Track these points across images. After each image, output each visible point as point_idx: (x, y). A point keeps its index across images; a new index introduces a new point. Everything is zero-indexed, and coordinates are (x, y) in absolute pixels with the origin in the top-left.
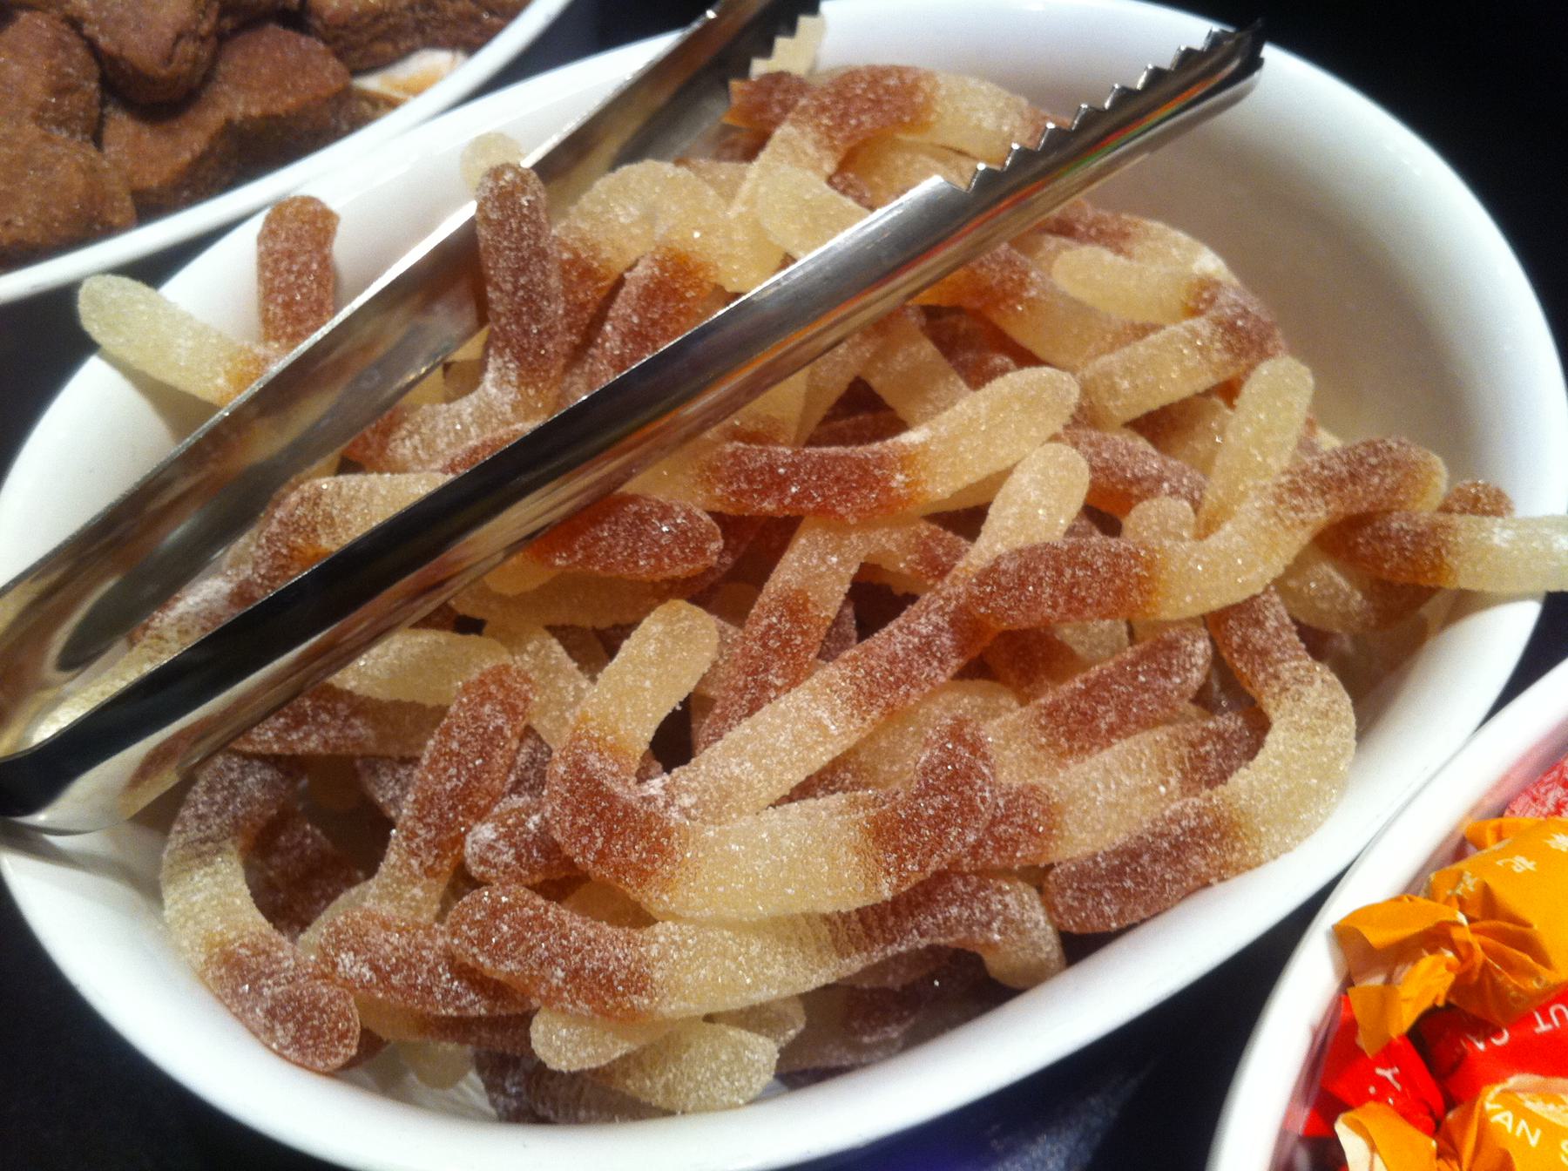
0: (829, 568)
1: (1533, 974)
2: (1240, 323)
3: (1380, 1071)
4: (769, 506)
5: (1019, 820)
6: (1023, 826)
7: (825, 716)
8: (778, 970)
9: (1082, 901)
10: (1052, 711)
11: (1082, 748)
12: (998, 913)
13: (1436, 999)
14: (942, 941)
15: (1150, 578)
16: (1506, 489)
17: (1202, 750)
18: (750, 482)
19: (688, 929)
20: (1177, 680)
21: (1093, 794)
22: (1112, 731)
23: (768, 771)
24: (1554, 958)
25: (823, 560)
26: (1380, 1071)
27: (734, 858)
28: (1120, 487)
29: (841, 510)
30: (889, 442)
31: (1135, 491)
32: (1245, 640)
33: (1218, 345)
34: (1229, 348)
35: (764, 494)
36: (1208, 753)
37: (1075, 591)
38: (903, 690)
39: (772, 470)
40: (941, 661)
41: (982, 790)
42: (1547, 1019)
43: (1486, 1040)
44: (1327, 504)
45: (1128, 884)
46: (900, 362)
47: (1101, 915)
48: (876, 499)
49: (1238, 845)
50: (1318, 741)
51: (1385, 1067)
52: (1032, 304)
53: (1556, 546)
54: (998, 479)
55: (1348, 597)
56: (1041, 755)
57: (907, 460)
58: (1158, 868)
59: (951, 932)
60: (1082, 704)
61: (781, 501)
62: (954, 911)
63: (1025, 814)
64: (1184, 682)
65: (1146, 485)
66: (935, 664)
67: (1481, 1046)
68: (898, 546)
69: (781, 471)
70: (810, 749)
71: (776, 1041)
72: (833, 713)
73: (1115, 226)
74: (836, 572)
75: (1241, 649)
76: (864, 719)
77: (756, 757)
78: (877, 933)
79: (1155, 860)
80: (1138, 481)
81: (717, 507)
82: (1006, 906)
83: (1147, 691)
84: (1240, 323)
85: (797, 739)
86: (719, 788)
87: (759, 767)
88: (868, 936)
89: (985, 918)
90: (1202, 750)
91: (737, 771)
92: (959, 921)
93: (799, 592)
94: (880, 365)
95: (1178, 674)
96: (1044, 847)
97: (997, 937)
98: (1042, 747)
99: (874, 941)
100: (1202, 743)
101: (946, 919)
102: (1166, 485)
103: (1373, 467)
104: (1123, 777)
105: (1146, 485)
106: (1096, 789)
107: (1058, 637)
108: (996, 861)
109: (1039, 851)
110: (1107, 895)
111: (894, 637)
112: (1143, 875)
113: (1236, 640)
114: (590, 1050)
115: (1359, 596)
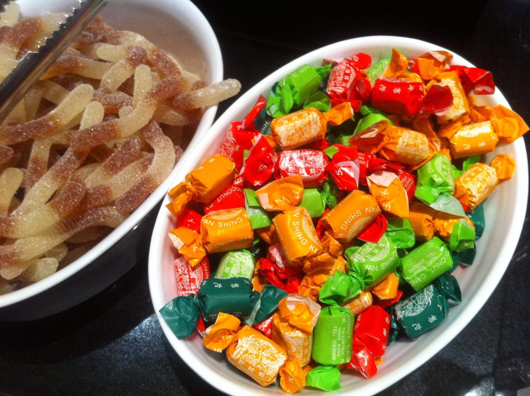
0: (42, 149)
1: (203, 190)
2: (134, 58)
3: (189, 221)
4: (20, 140)
5: (98, 193)
6: (99, 194)
7: (46, 184)
8: (45, 242)
9: (122, 206)
10: (105, 166)
11: (115, 172)
12: (101, 215)
13: (184, 201)
14: (88, 225)
15: (113, 129)
16: (322, 59)
17: (145, 164)
18: (13, 135)
19: (22, 240)
20: (133, 150)
21: (117, 182)
22: (121, 166)
23: (36, 201)
24: (207, 186)
25: (39, 148)
26: (189, 221)
27: (25, 222)
28: (114, 107)
29: (39, 135)
30: (48, 115)
31: (118, 107)
32: (148, 136)
33: (128, 65)
34: (131, 65)
35: (17, 137)
36: (146, 164)
37: (96, 137)
38: (65, 172)
39: (18, 131)
40: (74, 163)
41: (79, 189)
42: (220, 199)
43: (209, 207)
44: (155, 99)
45: (130, 199)
46: (51, 92)
47: (128, 208)
48: (47, 130)
49: (151, 183)
50: (163, 154)
51: (190, 219)
52: (83, 67)
53: (211, 92)
54: (80, 116)
55: (178, 117)
56: (106, 177)
57: (52, 118)
58: (135, 193)
59: (89, 222)
60: (112, 162)
61: (22, 138)
62: (89, 217)
63: (99, 191)
64: (135, 149)
65: (119, 105)
66: (72, 164)
67: (208, 209)
68: (60, 138)
69: (20, 131)
70: (45, 193)
71: (57, 259)
72: (48, 183)
73: (116, 35)
74: (44, 150)
75: (147, 138)
76: (57, 182)
77: (33, 198)
78: (70, 228)
79: (134, 192)
80: (117, 104)
81: (8, 144)
82: (104, 213)
83: (126, 154)
84: (134, 58)
85: (41, 191)
86: (27, 208)
87: (33, 200)
88: (68, 229)
89: (98, 217)
90: (145, 164)
91: (29, 203)
92: (90, 219)
93: (36, 157)
94: (47, 95)
95: (132, 148)
96: (108, 197)
97: (103, 220)
98: (106, 175)
99: (69, 229)
100: (144, 162)
101: (87, 220)
102: (124, 104)
103: (165, 86)
104: (125, 176)
105: (119, 105)
106: (118, 181)
107: (108, 148)
108: (96, 204)
109: (107, 198)
110: (127, 203)
111: (62, 161)
112: (133, 196)
113: (146, 136)
114: (13, 272)
115: (181, 116)
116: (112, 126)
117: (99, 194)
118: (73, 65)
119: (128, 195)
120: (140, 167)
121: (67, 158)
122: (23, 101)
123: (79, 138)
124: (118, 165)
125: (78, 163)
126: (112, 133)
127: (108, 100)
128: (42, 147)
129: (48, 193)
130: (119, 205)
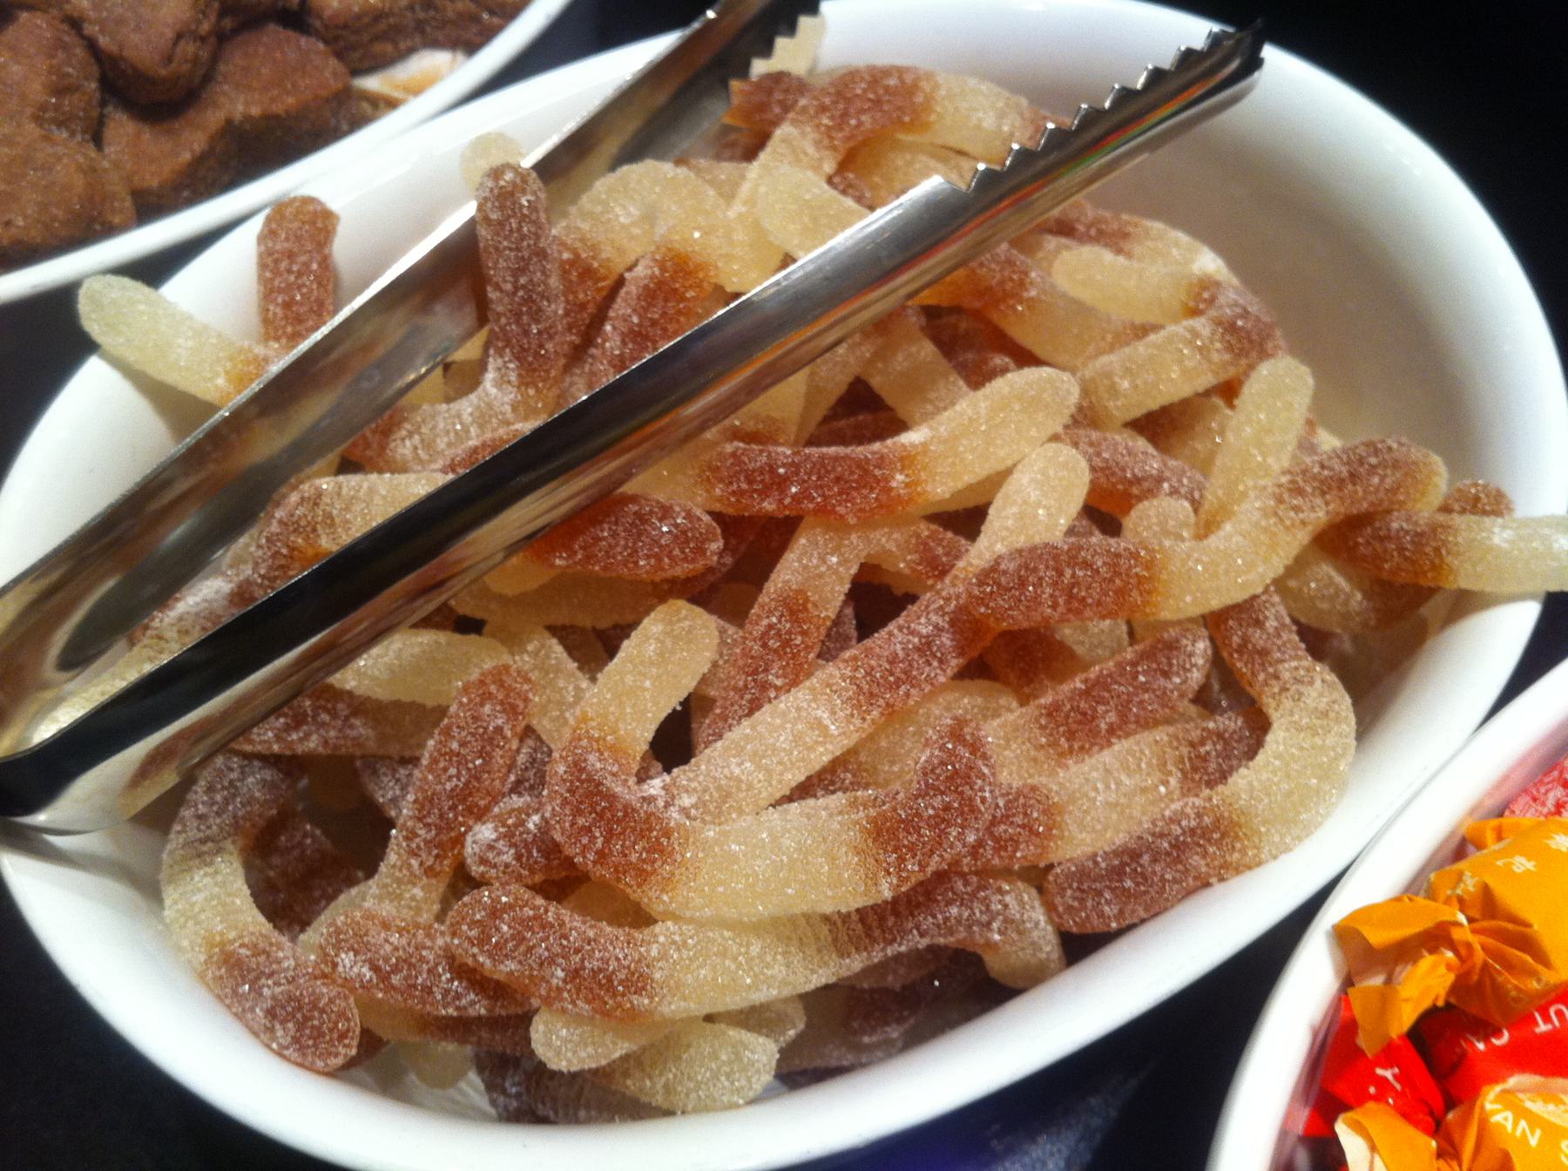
1: (1533, 974)
2: (1240, 323)
3: (1380, 1071)
4: (769, 506)
5: (1019, 820)
7: (825, 716)
8: (778, 970)
9: (1082, 901)
10: (1052, 711)
11: (1082, 748)
12: (998, 913)
13: (1436, 999)
14: (942, 941)
15: (1150, 578)
17: (1202, 750)
18: (750, 482)
19: (688, 929)
20: (1177, 680)
21: (1093, 794)
22: (1112, 731)
23: (768, 771)
24: (1554, 958)
25: (823, 560)
26: (1380, 1071)
27: (734, 858)
28: (1120, 487)
29: (841, 510)
30: (889, 442)
31: (1135, 491)
32: (1245, 640)
33: (1218, 345)
34: (1229, 348)
35: (764, 494)
36: (1208, 753)
37: (1075, 591)
38: (903, 690)
39: (772, 470)
40: (941, 661)
41: (982, 790)
42: (1547, 1019)
43: (1486, 1040)
44: (1327, 504)
45: (1128, 884)
46: (900, 362)
47: (1101, 915)
48: (876, 499)
50: (1318, 741)
51: (1385, 1067)
52: (1032, 304)
53: (1556, 546)
54: (998, 479)
55: (1348, 597)
56: (1041, 755)
57: (907, 460)
58: (1158, 868)
59: (951, 932)
60: (1082, 704)
61: (781, 501)
62: (954, 911)
63: (1025, 814)
64: (1184, 682)
65: (1146, 485)
66: (935, 664)
67: (1481, 1046)
69: (781, 471)
70: (810, 749)
71: (776, 1041)
72: (833, 713)
73: (1115, 226)
74: (836, 572)
75: (1241, 649)
76: (864, 719)
77: (756, 757)
78: (877, 933)
79: (1155, 860)
80: (1138, 481)
81: (717, 507)
84: (1240, 323)
85: (797, 739)
87: (759, 767)
88: (868, 936)
89: (985, 918)
90: (1202, 750)
91: (737, 771)
92: (959, 921)
93: (799, 592)
94: (880, 365)
95: (1178, 674)
96: (1044, 847)
97: (997, 937)
98: (1042, 747)
99: (874, 941)
101: (946, 919)
102: (1166, 485)
103: (1373, 467)
104: (1123, 777)
105: (1146, 485)
106: (1096, 789)
107: (1058, 637)
108: (996, 861)
109: (1039, 851)
110: (1107, 895)
111: (894, 637)
112: (1143, 875)
114: (590, 1050)
115: (1359, 596)
117: (1023, 826)
118: (1009, 286)
119: (1124, 864)
120: (1182, 757)
121: (921, 636)
123: (1020, 577)
124: (1103, 726)
125: (955, 663)
126: (1135, 593)
128: (835, 559)
129: (822, 754)
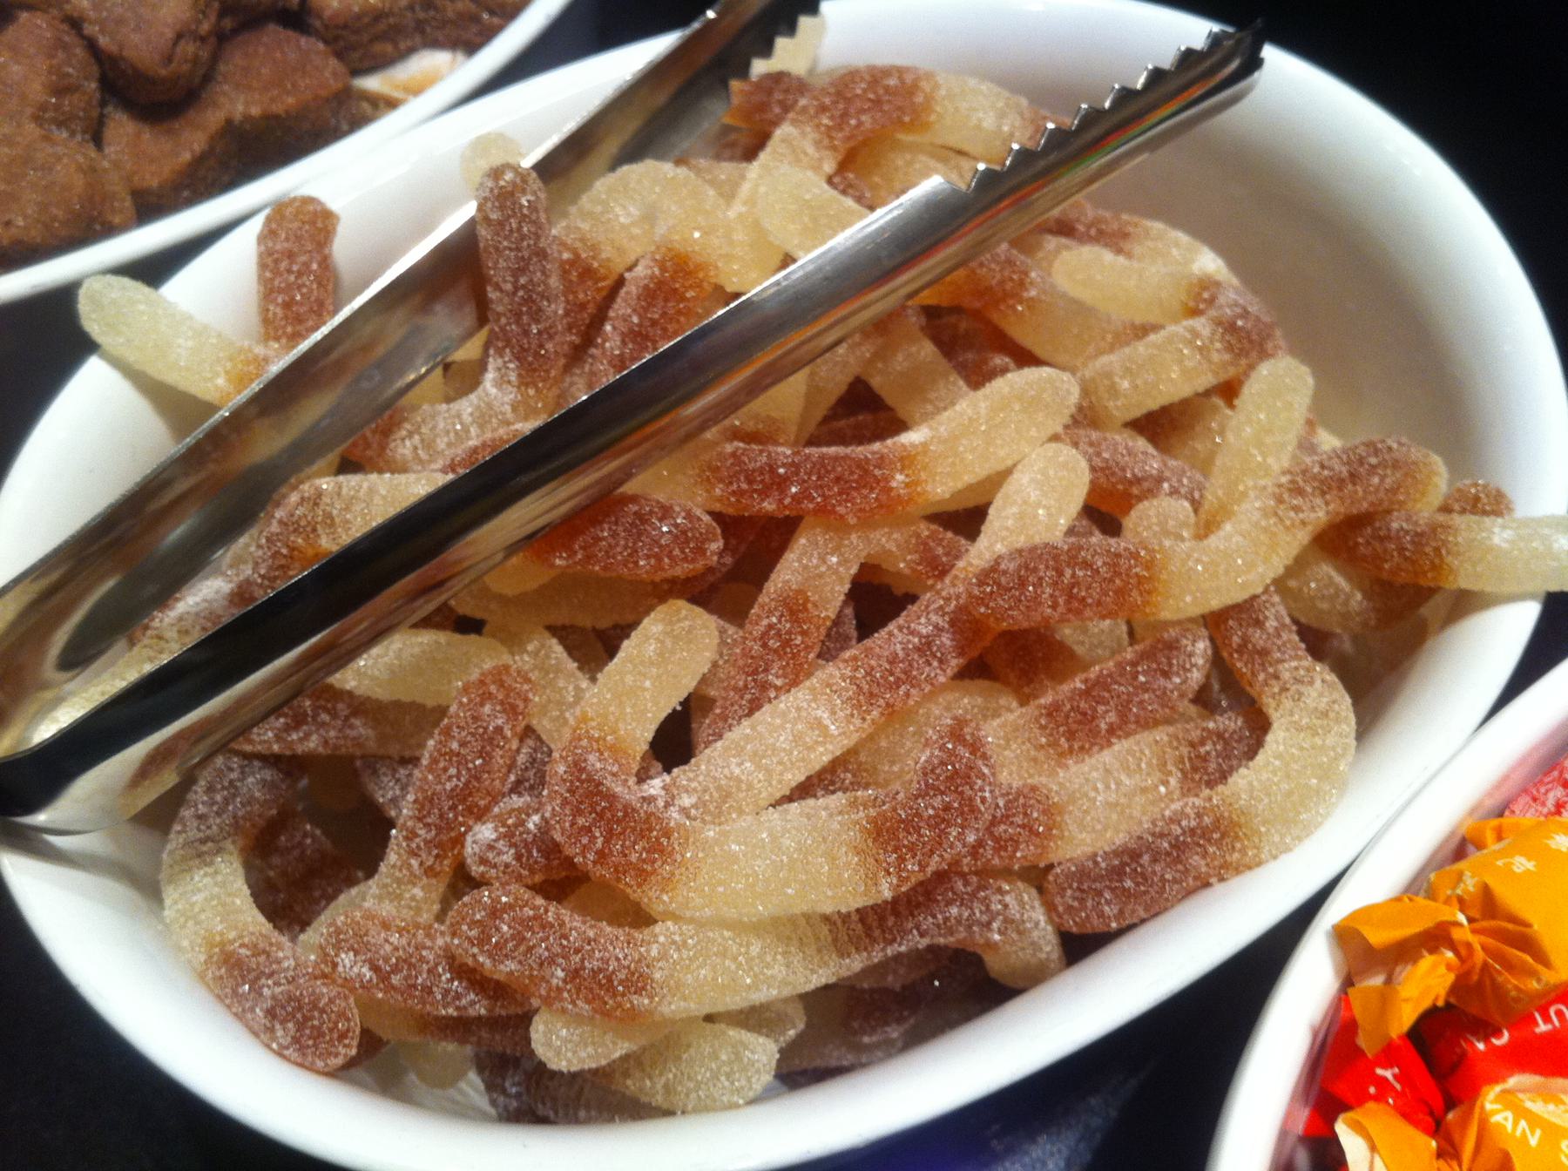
0: (829, 568)
1: (1533, 974)
2: (1240, 323)
3: (1380, 1071)
4: (769, 506)
5: (1019, 820)
6: (1023, 826)
7: (825, 716)
8: (778, 970)
9: (1082, 901)
10: (1052, 711)
11: (1082, 748)
12: (998, 913)
13: (1436, 999)
14: (942, 941)
15: (1150, 578)
17: (1202, 750)
19: (688, 929)
20: (1177, 680)
22: (1112, 731)
23: (768, 771)
24: (1554, 958)
25: (823, 560)
26: (1380, 1071)
27: (734, 858)
28: (1120, 487)
29: (841, 510)
30: (889, 442)
31: (1135, 491)
32: (1245, 640)
33: (1218, 345)
34: (1229, 348)
35: (764, 494)
37: (1075, 591)
38: (903, 690)
39: (772, 470)
40: (941, 661)
41: (982, 790)
42: (1547, 1019)
43: (1486, 1040)
44: (1327, 504)
45: (1128, 884)
46: (900, 362)
47: (1101, 915)
48: (876, 499)
49: (1238, 845)
50: (1318, 741)
51: (1385, 1067)
52: (1032, 304)
53: (1556, 546)
54: (998, 479)
55: (1348, 597)
56: (1041, 755)
57: (907, 460)
58: (1158, 868)
59: (951, 932)
60: (1082, 704)
61: (781, 501)
62: (954, 911)
63: (1025, 814)
64: (1184, 682)
65: (1146, 485)
66: (935, 664)
67: (1481, 1046)
70: (810, 749)
71: (776, 1041)
72: (833, 713)
73: (1115, 226)
74: (836, 572)
75: (1241, 649)
76: (864, 719)
77: (756, 757)
78: (877, 933)
79: (1155, 860)
80: (1138, 481)
81: (717, 507)
82: (1006, 906)
83: (1147, 691)
84: (1240, 323)
85: (797, 739)
86: (719, 788)
87: (759, 767)
88: (868, 936)
89: (985, 918)
90: (1202, 750)
91: (737, 771)
92: (959, 921)
94: (880, 365)
95: (1178, 674)
96: (1044, 847)
97: (997, 937)
98: (1042, 747)
99: (874, 941)
100: (1202, 743)
101: (946, 919)
102: (1166, 485)
103: (1373, 467)
105: (1146, 485)
106: (1096, 789)
108: (996, 861)
109: (1039, 851)
110: (1107, 895)
111: (894, 637)
112: (1143, 875)
114: (590, 1050)
115: (1359, 596)
116: (1149, 565)
117: (1023, 826)
119: (1124, 864)
120: (1182, 757)
122: (806, 371)
123: (1020, 577)
124: (1103, 726)
126: (1135, 593)
127: (1106, 455)
130: (1069, 892)
